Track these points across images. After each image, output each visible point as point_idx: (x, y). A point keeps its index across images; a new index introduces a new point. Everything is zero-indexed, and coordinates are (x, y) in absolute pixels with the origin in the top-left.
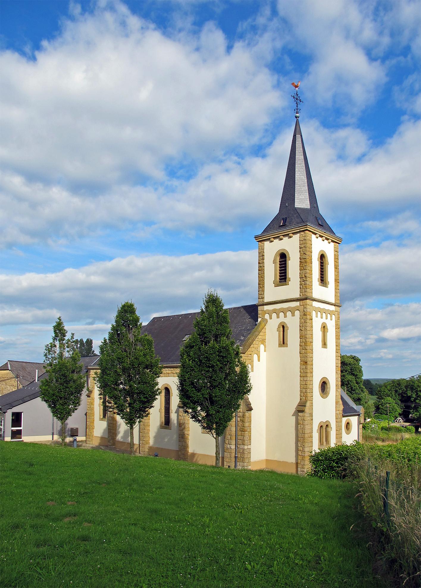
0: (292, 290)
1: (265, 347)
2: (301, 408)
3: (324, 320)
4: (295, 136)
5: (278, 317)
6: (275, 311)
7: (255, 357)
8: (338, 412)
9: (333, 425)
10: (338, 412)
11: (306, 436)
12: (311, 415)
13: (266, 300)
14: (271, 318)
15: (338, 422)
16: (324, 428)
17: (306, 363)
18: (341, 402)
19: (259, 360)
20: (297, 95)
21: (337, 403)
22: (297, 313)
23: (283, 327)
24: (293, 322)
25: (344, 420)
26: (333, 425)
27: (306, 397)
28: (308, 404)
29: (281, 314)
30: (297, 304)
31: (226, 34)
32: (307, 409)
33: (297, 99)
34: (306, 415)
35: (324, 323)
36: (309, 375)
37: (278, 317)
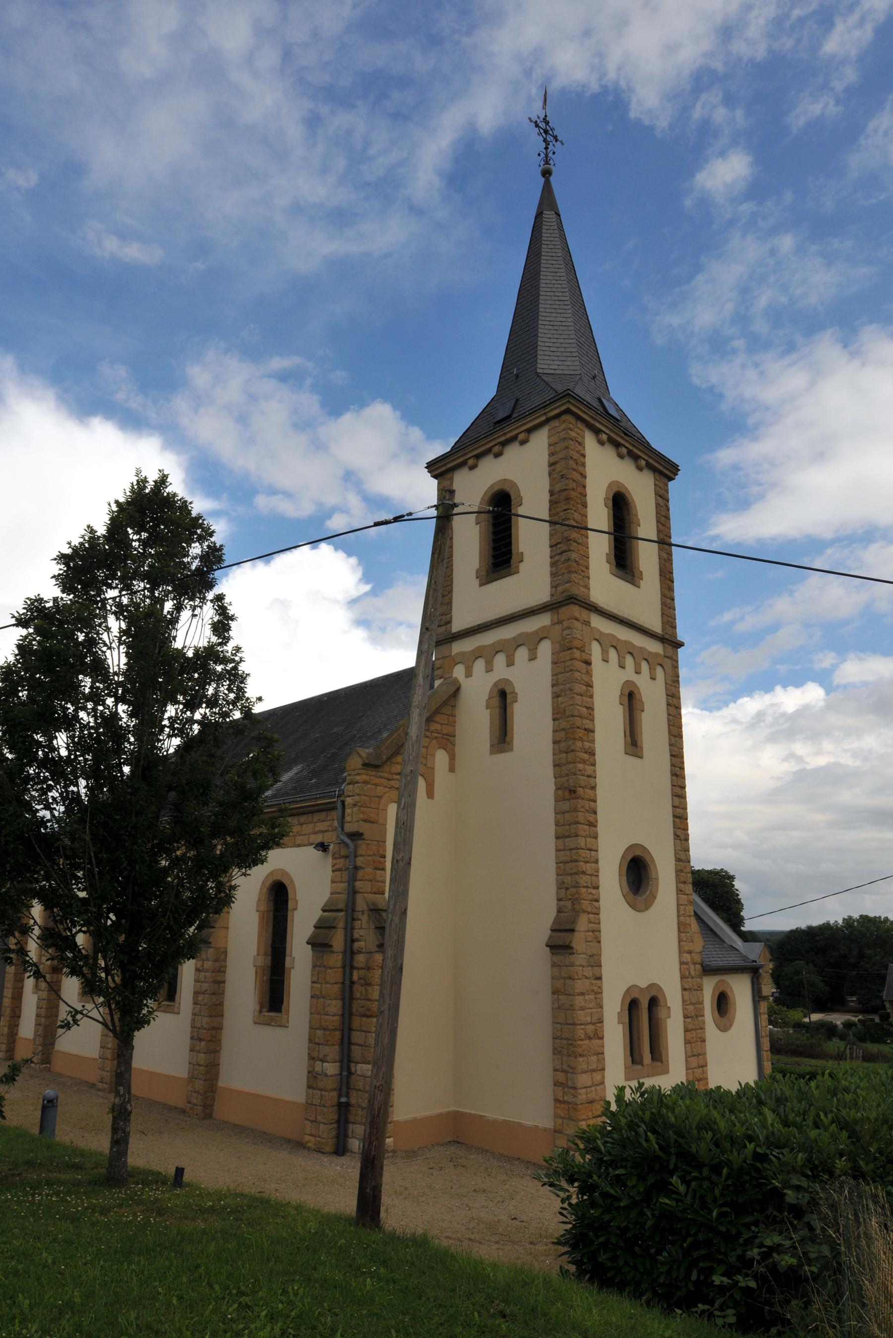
0: (531, 581)
1: (452, 758)
2: (562, 938)
3: (629, 674)
4: (539, 215)
5: (489, 669)
6: (478, 653)
7: (421, 784)
8: (687, 957)
9: (673, 999)
10: (687, 957)
11: (580, 1032)
12: (595, 962)
13: (457, 625)
14: (469, 674)
15: (690, 990)
16: (643, 1011)
17: (574, 793)
18: (695, 926)
19: (430, 794)
20: (547, 123)
21: (682, 928)
22: (545, 649)
23: (503, 694)
24: (532, 679)
25: (709, 988)
26: (673, 999)
27: (575, 900)
28: (582, 924)
29: (500, 660)
30: (545, 620)
31: (349, 554)
32: (579, 942)
33: (546, 132)
34: (579, 959)
35: (628, 683)
36: (583, 829)
37: (489, 669)
